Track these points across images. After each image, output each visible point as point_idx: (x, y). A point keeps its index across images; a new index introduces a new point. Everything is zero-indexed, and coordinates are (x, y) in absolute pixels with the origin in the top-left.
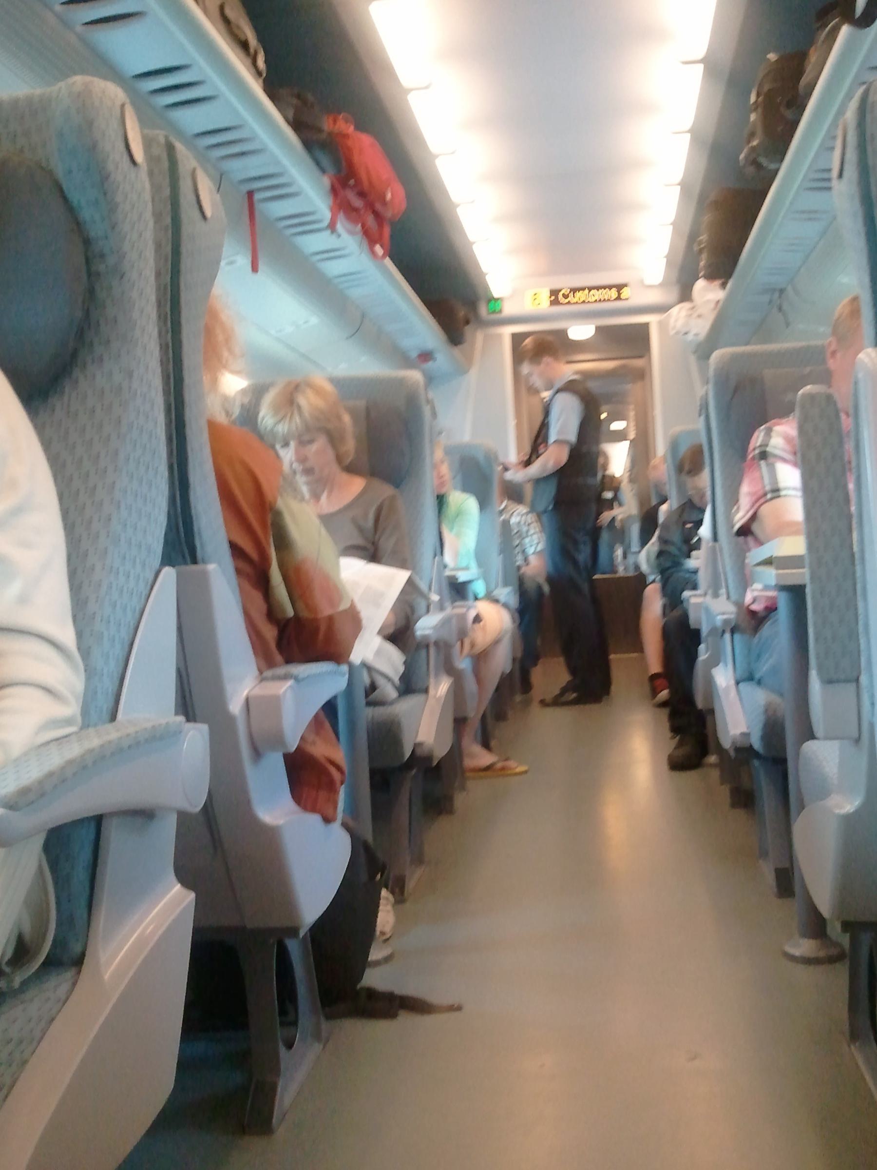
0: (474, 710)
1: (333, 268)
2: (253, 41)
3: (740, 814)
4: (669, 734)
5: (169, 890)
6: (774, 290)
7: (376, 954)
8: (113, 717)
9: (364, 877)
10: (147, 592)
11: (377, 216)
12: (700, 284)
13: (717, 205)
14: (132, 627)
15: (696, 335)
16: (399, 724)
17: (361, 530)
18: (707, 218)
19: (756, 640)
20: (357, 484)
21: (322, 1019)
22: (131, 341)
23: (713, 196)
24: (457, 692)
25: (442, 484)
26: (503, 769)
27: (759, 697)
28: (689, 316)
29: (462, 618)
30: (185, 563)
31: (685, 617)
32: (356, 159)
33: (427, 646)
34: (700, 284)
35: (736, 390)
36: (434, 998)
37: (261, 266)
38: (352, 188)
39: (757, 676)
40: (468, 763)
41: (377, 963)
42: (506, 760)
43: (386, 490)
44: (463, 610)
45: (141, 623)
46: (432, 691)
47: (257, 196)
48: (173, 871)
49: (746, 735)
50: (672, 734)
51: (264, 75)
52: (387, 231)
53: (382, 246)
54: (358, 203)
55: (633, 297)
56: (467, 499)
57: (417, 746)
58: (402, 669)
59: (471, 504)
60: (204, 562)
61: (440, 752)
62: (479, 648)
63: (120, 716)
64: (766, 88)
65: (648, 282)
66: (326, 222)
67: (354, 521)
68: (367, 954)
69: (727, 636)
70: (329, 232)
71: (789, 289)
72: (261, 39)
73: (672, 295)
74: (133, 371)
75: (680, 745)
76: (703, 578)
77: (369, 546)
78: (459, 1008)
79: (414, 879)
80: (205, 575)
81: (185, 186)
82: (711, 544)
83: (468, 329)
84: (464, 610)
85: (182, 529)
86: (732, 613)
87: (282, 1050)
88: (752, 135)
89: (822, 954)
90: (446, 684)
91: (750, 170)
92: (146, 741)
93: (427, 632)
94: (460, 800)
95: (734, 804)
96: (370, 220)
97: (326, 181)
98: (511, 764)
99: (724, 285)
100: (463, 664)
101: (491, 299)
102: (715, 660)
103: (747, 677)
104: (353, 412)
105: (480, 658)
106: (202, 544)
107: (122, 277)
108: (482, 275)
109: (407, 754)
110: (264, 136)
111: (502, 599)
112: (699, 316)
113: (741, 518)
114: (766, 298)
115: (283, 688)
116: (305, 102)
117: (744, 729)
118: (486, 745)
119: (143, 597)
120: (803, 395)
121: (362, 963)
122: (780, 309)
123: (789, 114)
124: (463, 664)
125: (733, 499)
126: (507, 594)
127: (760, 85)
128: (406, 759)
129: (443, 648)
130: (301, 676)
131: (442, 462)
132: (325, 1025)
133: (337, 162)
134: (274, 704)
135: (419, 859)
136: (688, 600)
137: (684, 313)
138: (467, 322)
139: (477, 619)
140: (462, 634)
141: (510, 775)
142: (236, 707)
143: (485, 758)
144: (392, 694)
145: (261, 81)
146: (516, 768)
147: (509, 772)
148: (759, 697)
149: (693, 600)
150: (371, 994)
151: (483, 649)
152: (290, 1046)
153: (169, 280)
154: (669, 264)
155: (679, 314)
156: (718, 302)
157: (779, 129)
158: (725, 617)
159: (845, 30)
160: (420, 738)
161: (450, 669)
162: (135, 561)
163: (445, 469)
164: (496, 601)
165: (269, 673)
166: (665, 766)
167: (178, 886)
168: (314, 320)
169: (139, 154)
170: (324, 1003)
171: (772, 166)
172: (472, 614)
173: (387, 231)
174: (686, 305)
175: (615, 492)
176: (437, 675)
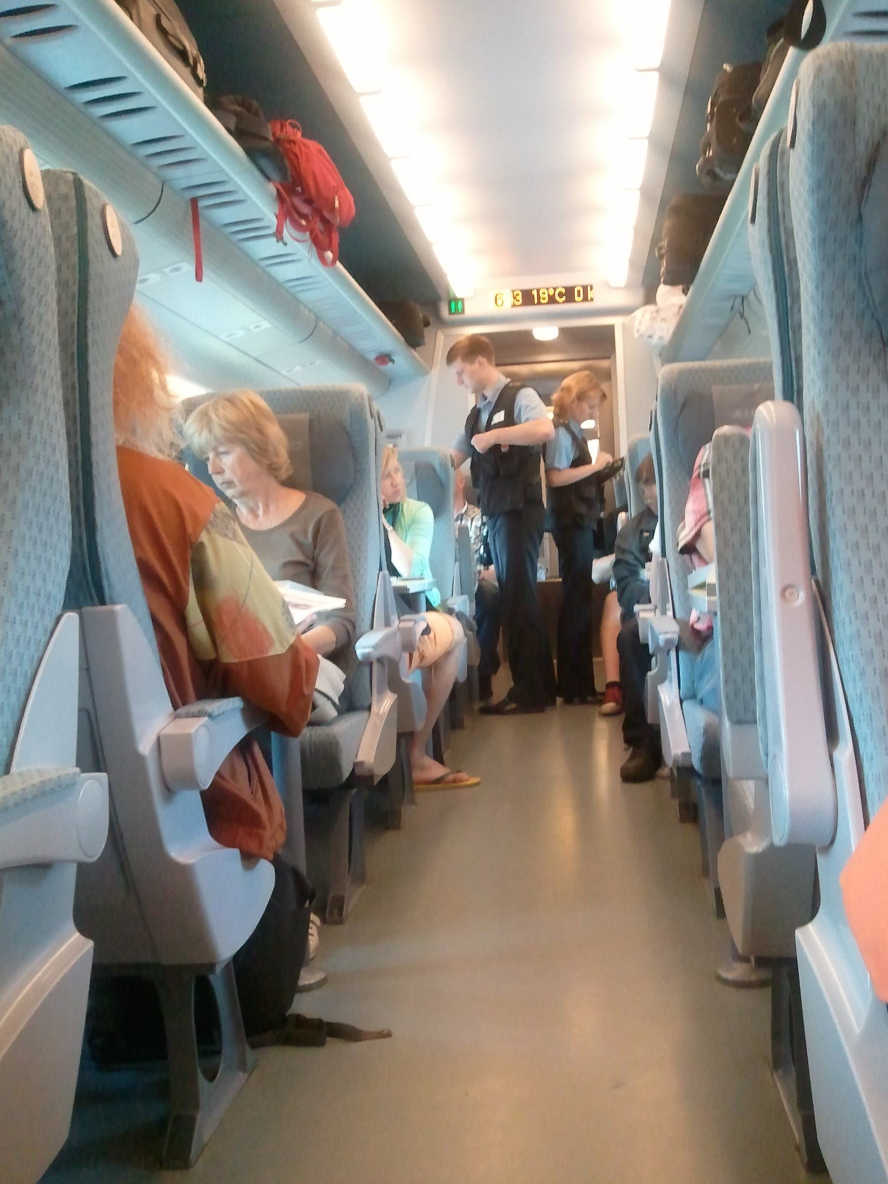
0: (422, 724)
1: (284, 273)
2: (192, 48)
3: (689, 827)
4: (624, 746)
5: (69, 937)
6: (736, 297)
7: (307, 978)
8: (7, 771)
9: (293, 906)
10: (44, 640)
11: (326, 222)
12: (663, 290)
13: (676, 211)
14: (29, 674)
15: (661, 338)
16: (337, 744)
17: (300, 545)
18: (667, 224)
19: (699, 659)
20: (295, 500)
21: (248, 1047)
22: (31, 387)
23: (673, 201)
24: (403, 707)
25: (396, 493)
26: (454, 781)
27: (699, 717)
28: (653, 319)
29: (409, 632)
30: (94, 605)
31: (635, 633)
32: (303, 165)
33: (371, 664)
34: (663, 290)
35: (684, 405)
36: (362, 1025)
37: (205, 271)
38: (298, 194)
39: (699, 696)
40: (417, 775)
41: (309, 988)
42: (459, 771)
43: (326, 505)
44: (411, 624)
45: (40, 669)
46: (374, 708)
47: (202, 204)
48: (72, 917)
49: (687, 755)
50: (626, 745)
51: (205, 85)
52: (336, 238)
53: (332, 252)
54: (305, 209)
55: (601, 298)
56: (422, 507)
57: (355, 765)
58: (342, 687)
59: (426, 512)
60: (113, 602)
61: (382, 770)
62: (429, 660)
63: (14, 769)
64: (721, 98)
65: (613, 284)
66: (274, 229)
67: (293, 536)
68: (296, 977)
69: (673, 654)
70: (274, 239)
71: (752, 297)
72: (201, 49)
73: (638, 296)
74: (32, 417)
75: (633, 757)
76: (654, 592)
77: (309, 562)
78: (388, 1035)
79: (354, 898)
80: (112, 615)
81: (94, 223)
82: (660, 559)
83: (427, 332)
84: (411, 624)
85: (88, 570)
86: (674, 633)
87: (202, 1081)
88: (708, 145)
89: (754, 978)
90: (389, 701)
91: (706, 180)
92: (35, 797)
93: (367, 650)
94: (408, 813)
95: (683, 819)
96: (319, 226)
97: (272, 188)
98: (463, 775)
99: (685, 291)
100: (412, 677)
101: (452, 300)
102: (662, 678)
103: (689, 696)
104: (289, 429)
105: (431, 670)
106: (109, 584)
107: (21, 323)
108: (443, 276)
109: (346, 774)
110: (205, 146)
111: (457, 608)
112: (664, 320)
113: (686, 535)
114: (729, 305)
115: (194, 727)
116: (249, 108)
117: (686, 749)
118: (438, 757)
119: (42, 644)
120: (717, 436)
121: (292, 988)
122: (742, 315)
123: (743, 126)
124: (412, 677)
125: (679, 517)
126: (463, 603)
127: (716, 96)
128: (344, 780)
129: (389, 665)
130: (216, 713)
131: (397, 470)
132: (251, 1055)
133: (282, 170)
134: (185, 743)
135: (360, 878)
136: (638, 614)
137: (648, 316)
138: (427, 324)
139: (427, 631)
140: (409, 647)
141: (460, 787)
142: (145, 747)
143: (436, 770)
144: (333, 713)
145: (201, 91)
146: (467, 780)
147: (462, 784)
148: (699, 717)
149: (642, 615)
150: (300, 1021)
151: (433, 661)
152: (211, 1076)
153: (76, 320)
154: (633, 264)
155: (643, 316)
156: (681, 307)
157: (735, 140)
158: (668, 636)
159: (792, 51)
160: (361, 758)
161: (395, 684)
162: (33, 609)
163: (399, 478)
164: (450, 611)
165: (182, 710)
166: (619, 779)
167: (77, 935)
168: (266, 325)
169: (39, 199)
170: (248, 1035)
171: (728, 177)
172: (422, 626)
173: (336, 238)
174: (650, 308)
175: (540, 302)
176: (380, 692)
